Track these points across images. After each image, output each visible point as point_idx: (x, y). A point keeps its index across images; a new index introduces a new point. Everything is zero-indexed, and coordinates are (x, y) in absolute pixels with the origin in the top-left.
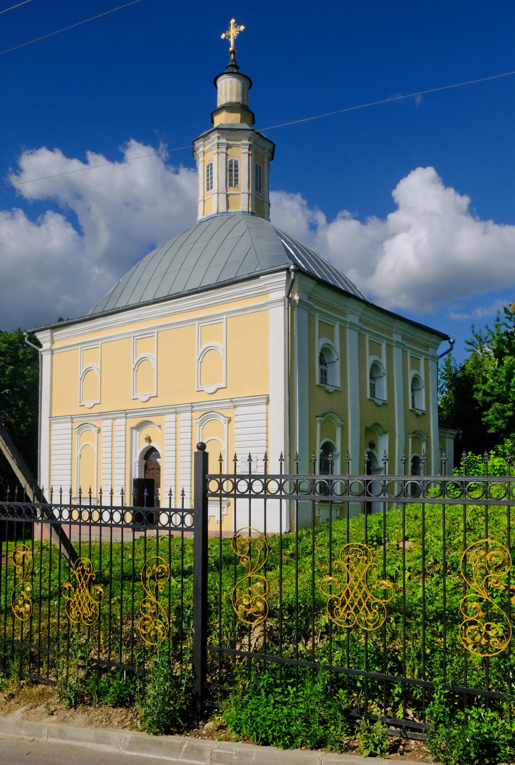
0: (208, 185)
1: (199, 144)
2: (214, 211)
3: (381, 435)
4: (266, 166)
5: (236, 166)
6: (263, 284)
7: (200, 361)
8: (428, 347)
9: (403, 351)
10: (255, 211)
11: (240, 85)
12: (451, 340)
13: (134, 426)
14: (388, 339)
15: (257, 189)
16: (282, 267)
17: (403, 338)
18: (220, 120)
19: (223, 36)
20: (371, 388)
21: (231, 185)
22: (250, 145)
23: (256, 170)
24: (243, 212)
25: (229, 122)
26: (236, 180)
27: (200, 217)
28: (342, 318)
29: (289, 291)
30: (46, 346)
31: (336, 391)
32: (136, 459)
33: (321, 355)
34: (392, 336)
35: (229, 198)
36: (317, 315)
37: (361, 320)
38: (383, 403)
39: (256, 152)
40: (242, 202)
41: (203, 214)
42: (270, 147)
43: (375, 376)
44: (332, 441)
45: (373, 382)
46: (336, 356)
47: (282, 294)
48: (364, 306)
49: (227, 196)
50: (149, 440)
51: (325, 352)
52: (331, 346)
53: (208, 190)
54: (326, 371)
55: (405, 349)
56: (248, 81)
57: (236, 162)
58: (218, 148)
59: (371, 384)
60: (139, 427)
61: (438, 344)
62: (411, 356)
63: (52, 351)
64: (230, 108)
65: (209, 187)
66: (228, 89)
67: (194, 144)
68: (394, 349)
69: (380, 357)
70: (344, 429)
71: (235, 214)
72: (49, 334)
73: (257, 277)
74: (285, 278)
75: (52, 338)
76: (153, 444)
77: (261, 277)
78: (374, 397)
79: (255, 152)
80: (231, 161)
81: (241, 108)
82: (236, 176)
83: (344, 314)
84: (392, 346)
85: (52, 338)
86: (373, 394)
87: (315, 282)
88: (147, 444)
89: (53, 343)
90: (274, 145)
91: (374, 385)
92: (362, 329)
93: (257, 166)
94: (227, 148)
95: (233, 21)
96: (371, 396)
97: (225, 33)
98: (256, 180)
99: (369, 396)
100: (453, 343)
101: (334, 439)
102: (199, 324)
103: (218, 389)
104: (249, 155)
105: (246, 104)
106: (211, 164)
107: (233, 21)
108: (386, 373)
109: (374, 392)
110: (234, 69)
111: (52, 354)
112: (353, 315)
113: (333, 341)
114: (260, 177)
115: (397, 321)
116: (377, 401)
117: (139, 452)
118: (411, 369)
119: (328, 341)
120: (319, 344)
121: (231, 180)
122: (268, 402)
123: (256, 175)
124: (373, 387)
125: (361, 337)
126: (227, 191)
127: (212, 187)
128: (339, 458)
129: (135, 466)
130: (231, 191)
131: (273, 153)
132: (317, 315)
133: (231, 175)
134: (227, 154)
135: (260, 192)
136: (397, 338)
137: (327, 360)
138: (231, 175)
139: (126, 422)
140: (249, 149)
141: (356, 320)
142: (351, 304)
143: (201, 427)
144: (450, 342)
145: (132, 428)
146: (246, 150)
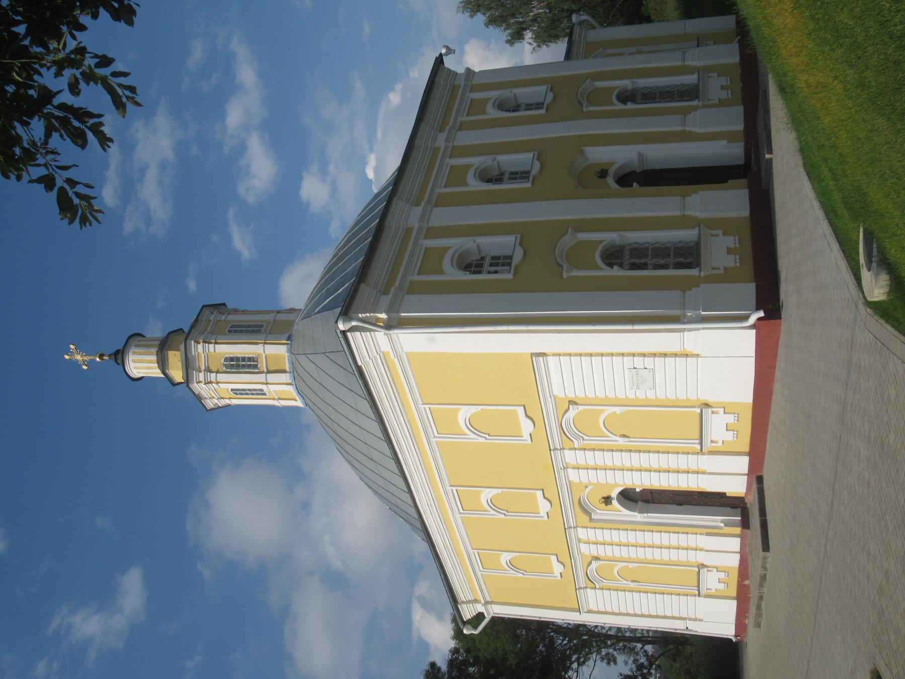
0: (258, 394)
1: (210, 404)
2: (291, 389)
3: (587, 159)
4: (230, 318)
5: (232, 359)
6: (370, 361)
7: (487, 436)
8: (454, 86)
9: (460, 129)
10: (286, 335)
11: (138, 350)
12: (444, 51)
13: (588, 519)
14: (418, 237)
15: (259, 332)
16: (342, 339)
17: (441, 130)
18: (177, 375)
19: (85, 367)
20: (532, 109)
21: (256, 367)
22: (205, 342)
23: (236, 332)
24: (290, 351)
25: (180, 365)
26: (250, 359)
27: (299, 403)
28: (442, 151)
29: (375, 323)
30: (480, 608)
31: (521, 245)
32: (637, 517)
33: (489, 181)
34: (459, 86)
35: (271, 368)
36: (460, 119)
37: (417, 204)
38: (538, 159)
39: (213, 334)
40: (277, 351)
41: (296, 400)
42: (206, 312)
43: (497, 173)
44: (615, 93)
45: (523, 107)
46: (507, 93)
47: (380, 336)
48: (395, 199)
49: (269, 372)
50: (607, 500)
51: (487, 177)
52: (478, 168)
53: (265, 394)
54: (512, 173)
55: (458, 124)
56: (133, 338)
57: (226, 359)
58: (211, 382)
59: (526, 110)
60: (588, 513)
61: (449, 70)
62: (419, 274)
63: (487, 603)
64: (163, 364)
65: (261, 393)
66: (141, 365)
67: (211, 410)
68: (457, 143)
69: (469, 167)
70: (580, 226)
71: (292, 363)
72: (464, 606)
73: (359, 369)
74: (358, 333)
75: (469, 602)
76: (614, 494)
77: (360, 364)
78: (543, 104)
79: (214, 335)
80: (226, 366)
81: (163, 347)
82: (243, 359)
83: (409, 231)
84: (454, 147)
85: (469, 602)
86: (539, 106)
87: (362, 285)
88: (615, 502)
89: (476, 601)
90: (204, 306)
91: (527, 105)
92: (429, 202)
93: (230, 331)
94: (211, 372)
95: (67, 357)
96: (542, 108)
97: (81, 366)
98: (247, 332)
99: (542, 112)
100: (447, 48)
101: (597, 243)
102: (435, 437)
103: (527, 416)
104: (216, 343)
105: (158, 343)
106: (232, 390)
107: (67, 357)
108: (492, 157)
109: (537, 104)
110: (119, 356)
111: (492, 603)
112: (409, 216)
113: (448, 248)
114: (244, 326)
115: (416, 143)
116: (534, 172)
117: (625, 511)
118: (467, 185)
119: (471, 172)
120: (453, 274)
121: (249, 366)
122: (543, 355)
123: (241, 332)
124: (529, 107)
125: (442, 201)
126: (263, 372)
127: (262, 390)
128: (636, 80)
129: (648, 517)
130: (263, 366)
131: (215, 306)
132: (460, 119)
133: (244, 366)
134: (218, 372)
135: (262, 326)
136: (441, 141)
137: (477, 257)
138: (244, 366)
139: (583, 527)
140: (210, 343)
141: (443, 136)
142: (393, 220)
143: (585, 437)
144: (447, 54)
145: (591, 520)
146: (211, 346)
